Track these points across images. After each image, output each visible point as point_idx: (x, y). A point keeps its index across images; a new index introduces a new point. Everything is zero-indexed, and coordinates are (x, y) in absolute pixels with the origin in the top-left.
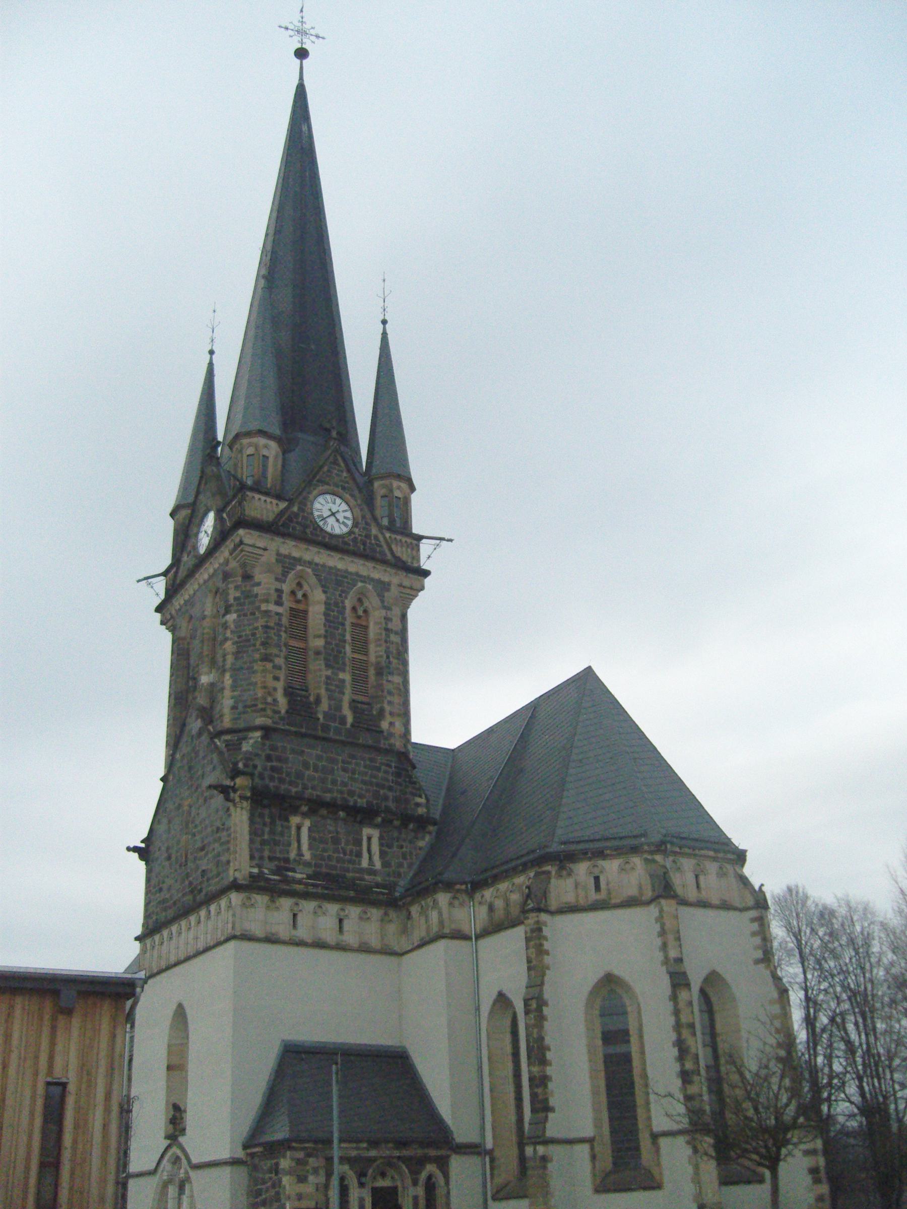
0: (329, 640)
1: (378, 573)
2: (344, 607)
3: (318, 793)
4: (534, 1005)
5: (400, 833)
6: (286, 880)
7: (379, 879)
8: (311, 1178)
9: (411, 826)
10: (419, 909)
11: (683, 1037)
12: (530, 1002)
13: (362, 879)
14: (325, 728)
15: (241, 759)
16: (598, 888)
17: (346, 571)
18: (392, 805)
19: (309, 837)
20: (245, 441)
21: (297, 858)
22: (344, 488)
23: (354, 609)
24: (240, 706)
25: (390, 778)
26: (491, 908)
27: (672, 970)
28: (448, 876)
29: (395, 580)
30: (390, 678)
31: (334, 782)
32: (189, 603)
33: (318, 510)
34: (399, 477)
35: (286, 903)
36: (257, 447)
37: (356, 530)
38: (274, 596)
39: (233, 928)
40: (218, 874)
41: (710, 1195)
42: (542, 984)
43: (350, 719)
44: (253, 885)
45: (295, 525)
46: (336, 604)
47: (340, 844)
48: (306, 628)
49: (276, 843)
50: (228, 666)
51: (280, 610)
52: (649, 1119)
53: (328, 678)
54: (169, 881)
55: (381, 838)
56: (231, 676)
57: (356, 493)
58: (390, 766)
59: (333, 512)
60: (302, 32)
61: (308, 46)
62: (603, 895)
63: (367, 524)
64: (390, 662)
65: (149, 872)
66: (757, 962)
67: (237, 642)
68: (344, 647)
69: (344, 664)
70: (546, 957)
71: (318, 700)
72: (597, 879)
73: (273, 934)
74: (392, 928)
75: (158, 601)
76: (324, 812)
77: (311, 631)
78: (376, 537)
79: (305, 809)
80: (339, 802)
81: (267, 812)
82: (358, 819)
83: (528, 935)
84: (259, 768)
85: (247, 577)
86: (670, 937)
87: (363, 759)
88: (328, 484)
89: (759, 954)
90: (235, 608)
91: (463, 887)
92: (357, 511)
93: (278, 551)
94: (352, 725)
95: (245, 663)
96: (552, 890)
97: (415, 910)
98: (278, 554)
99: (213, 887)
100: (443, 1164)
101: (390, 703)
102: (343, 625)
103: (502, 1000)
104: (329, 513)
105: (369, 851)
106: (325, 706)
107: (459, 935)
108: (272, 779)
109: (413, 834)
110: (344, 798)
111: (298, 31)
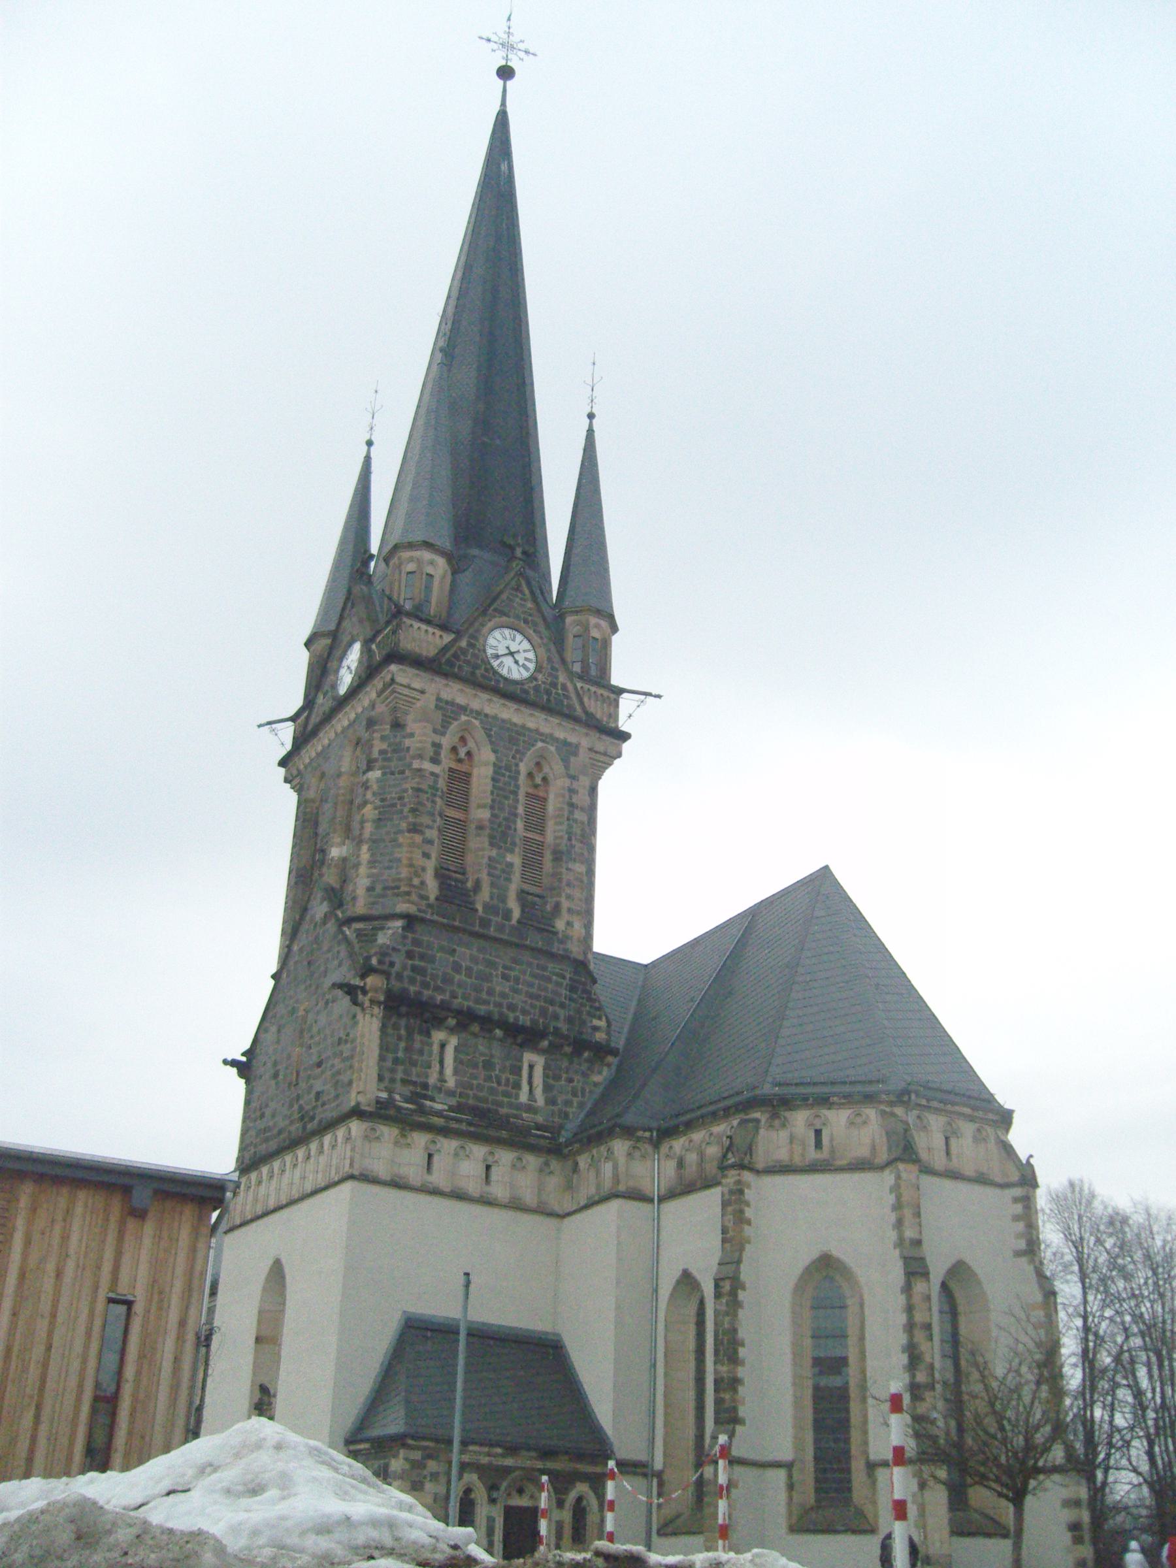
4: (727, 1286)
5: (571, 1063)
6: (422, 1110)
7: (540, 1119)
8: (429, 1486)
9: (586, 1054)
12: (721, 1284)
14: (485, 923)
15: (376, 954)
16: (818, 1144)
18: (564, 1027)
20: (406, 554)
22: (526, 621)
23: (530, 775)
26: (681, 1164)
28: (629, 1119)
29: (585, 743)
31: (490, 992)
32: (323, 755)
33: (493, 647)
34: (599, 613)
35: (420, 1139)
36: (419, 561)
38: (430, 752)
39: (351, 1165)
40: (337, 1097)
41: (938, 1544)
43: (516, 914)
44: (380, 1113)
45: (462, 665)
46: (508, 768)
52: (866, 1443)
53: (490, 858)
54: (273, 1105)
55: (546, 1068)
56: (369, 850)
57: (542, 628)
58: (564, 977)
59: (511, 652)
60: (508, 46)
62: (825, 1154)
63: (553, 668)
64: (573, 846)
65: (249, 1093)
66: (1018, 1254)
68: (515, 823)
69: (514, 844)
70: (746, 1227)
72: (818, 1133)
74: (553, 1182)
78: (564, 687)
80: (496, 1017)
81: (403, 1022)
82: (519, 1040)
84: (397, 967)
85: (397, 725)
86: (908, 1213)
87: (530, 964)
88: (505, 615)
89: (1022, 1244)
91: (647, 1134)
93: (438, 694)
98: (439, 699)
99: (329, 1113)
100: (597, 1482)
101: (569, 897)
102: (515, 793)
103: (687, 1280)
105: (530, 1083)
106: (485, 895)
107: (636, 1196)
108: (412, 981)
110: (501, 1014)
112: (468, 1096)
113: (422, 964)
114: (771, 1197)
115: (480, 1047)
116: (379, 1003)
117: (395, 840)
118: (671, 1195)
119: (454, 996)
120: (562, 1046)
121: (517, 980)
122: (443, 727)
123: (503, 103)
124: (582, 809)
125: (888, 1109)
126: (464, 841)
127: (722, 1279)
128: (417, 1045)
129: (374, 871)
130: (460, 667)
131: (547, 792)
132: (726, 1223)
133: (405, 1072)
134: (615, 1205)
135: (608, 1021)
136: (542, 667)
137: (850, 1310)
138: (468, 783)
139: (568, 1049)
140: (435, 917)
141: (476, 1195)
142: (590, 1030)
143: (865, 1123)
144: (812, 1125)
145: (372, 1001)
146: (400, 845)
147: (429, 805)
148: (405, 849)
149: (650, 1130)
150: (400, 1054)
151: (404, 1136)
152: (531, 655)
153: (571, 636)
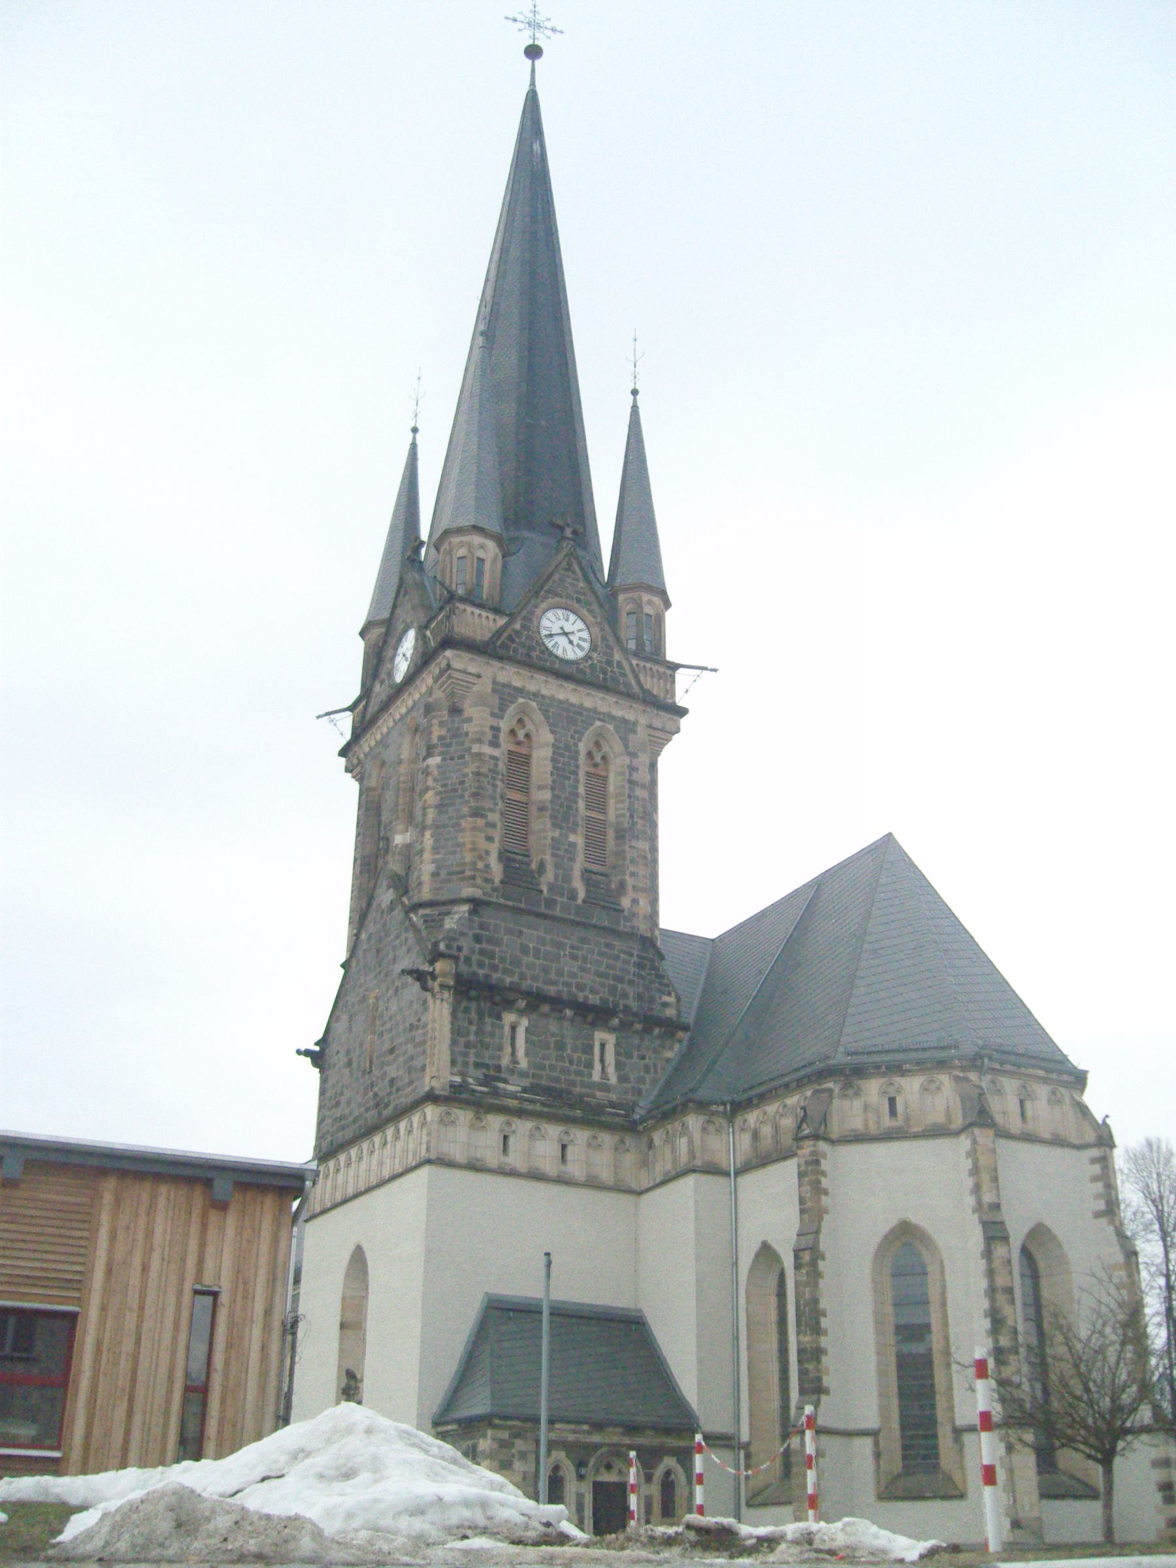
2: (577, 752)
4: (806, 1256)
5: (642, 1040)
6: (496, 1093)
7: (613, 1097)
8: (518, 1465)
9: (657, 1031)
11: (998, 1304)
12: (801, 1254)
13: (594, 1096)
14: (551, 903)
15: (443, 940)
16: (893, 1112)
17: (581, 707)
18: (633, 1004)
20: (456, 540)
22: (579, 601)
23: (590, 754)
24: (443, 872)
25: (632, 969)
26: (756, 1136)
27: (985, 1218)
28: (702, 1093)
31: (559, 972)
32: (383, 743)
33: (546, 628)
35: (495, 1122)
36: (469, 546)
37: (595, 655)
38: (489, 736)
40: (411, 1083)
42: (818, 1232)
43: (582, 894)
44: (455, 1096)
48: (528, 777)
51: (496, 753)
52: (951, 1408)
53: (553, 839)
54: (348, 1094)
55: (617, 1045)
57: (595, 607)
59: (565, 632)
60: (534, 25)
62: (900, 1121)
63: (607, 646)
64: (634, 824)
65: (323, 1081)
66: (1097, 1215)
67: (440, 793)
68: (576, 803)
69: (576, 824)
70: (823, 1197)
71: (542, 866)
72: (892, 1101)
73: (478, 1160)
74: (629, 1159)
75: (342, 742)
76: (546, 1008)
77: (535, 780)
78: (619, 664)
79: (522, 1004)
80: (565, 996)
81: (474, 1005)
82: (589, 1019)
83: (803, 1168)
84: (465, 952)
86: (985, 1177)
89: (1101, 1205)
90: (440, 749)
91: (721, 1108)
92: (596, 630)
95: (450, 818)
99: (405, 1099)
102: (576, 773)
103: (766, 1252)
104: (560, 631)
105: (602, 1060)
106: (550, 875)
108: (481, 965)
109: (658, 1042)
110: (570, 992)
111: (529, 24)
112: (541, 1077)
116: (448, 987)
117: (458, 824)
119: (523, 977)
121: (585, 959)
123: (533, 83)
125: (961, 1075)
127: (803, 1250)
128: (488, 1028)
129: (437, 856)
130: (516, 651)
133: (477, 1055)
134: (691, 1179)
135: (678, 999)
136: (596, 646)
140: (502, 901)
145: (442, 986)
146: (462, 830)
150: (472, 1038)
152: (585, 635)
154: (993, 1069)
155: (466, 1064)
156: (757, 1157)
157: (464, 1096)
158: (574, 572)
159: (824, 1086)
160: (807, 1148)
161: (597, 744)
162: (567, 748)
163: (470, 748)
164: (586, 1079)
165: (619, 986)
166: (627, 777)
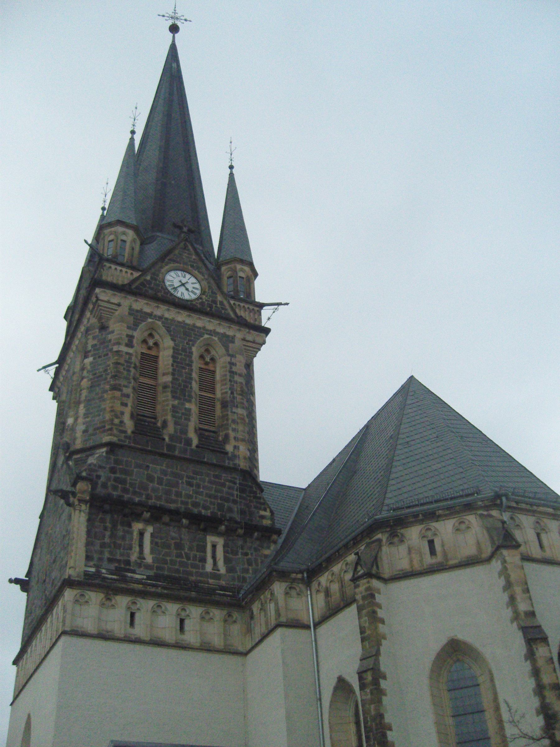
0: (176, 376)
1: (222, 328)
3: (162, 503)
5: (245, 542)
6: (124, 579)
7: (223, 583)
9: (256, 534)
10: (260, 606)
11: (548, 701)
12: (364, 675)
14: (171, 447)
15: (85, 470)
16: (433, 552)
17: (194, 325)
18: (237, 517)
19: (152, 543)
20: (107, 231)
21: (139, 561)
22: (192, 266)
23: (202, 357)
24: (91, 431)
26: (327, 593)
27: (523, 624)
29: (239, 335)
30: (234, 410)
31: (178, 494)
33: (169, 281)
34: (242, 262)
35: (123, 601)
36: (116, 234)
37: (204, 297)
38: (126, 340)
39: (64, 625)
42: (378, 654)
43: (195, 442)
44: (87, 582)
47: (184, 549)
48: (157, 369)
49: (118, 546)
50: (83, 398)
51: (131, 351)
53: (173, 406)
56: (85, 407)
57: (204, 270)
58: (235, 483)
59: (184, 284)
61: (179, 23)
62: (439, 558)
67: (91, 379)
68: (191, 384)
69: (190, 396)
70: (381, 625)
71: (165, 423)
72: (431, 543)
73: (108, 632)
74: (236, 629)
75: (50, 381)
76: (166, 518)
77: (160, 371)
78: (221, 303)
79: (147, 515)
80: (183, 510)
81: (108, 517)
82: (202, 527)
84: (103, 479)
86: (518, 590)
87: (208, 475)
88: (177, 262)
90: (92, 353)
91: (299, 576)
92: (205, 283)
93: (131, 306)
94: (197, 446)
95: (97, 394)
96: (384, 558)
97: (256, 607)
102: (190, 366)
104: (180, 284)
105: (214, 557)
106: (171, 429)
108: (115, 488)
109: (258, 543)
112: (163, 569)
113: (124, 476)
114: (397, 600)
115: (173, 534)
116: (85, 502)
117: (102, 397)
118: (324, 619)
119: (148, 497)
120: (236, 530)
121: (198, 486)
122: (134, 325)
124: (240, 375)
125: (485, 513)
126: (154, 398)
127: (365, 671)
128: (120, 533)
129: (87, 419)
131: (215, 367)
132: (363, 625)
133: (111, 553)
134: (279, 632)
135: (272, 512)
137: (482, 687)
138: (156, 362)
139: (241, 531)
141: (172, 641)
142: (258, 519)
143: (468, 527)
144: (424, 537)
145: (80, 501)
146: (104, 400)
147: (125, 373)
148: (108, 402)
149: (301, 572)
150: (107, 540)
151: (109, 599)
153: (225, 278)
154: (509, 507)
155: (100, 559)
156: (329, 609)
157: (97, 581)
158: (188, 250)
159: (375, 538)
160: (363, 584)
161: (207, 351)
162: (184, 350)
163: (112, 349)
164: (201, 571)
165: (226, 504)
166: (228, 369)
